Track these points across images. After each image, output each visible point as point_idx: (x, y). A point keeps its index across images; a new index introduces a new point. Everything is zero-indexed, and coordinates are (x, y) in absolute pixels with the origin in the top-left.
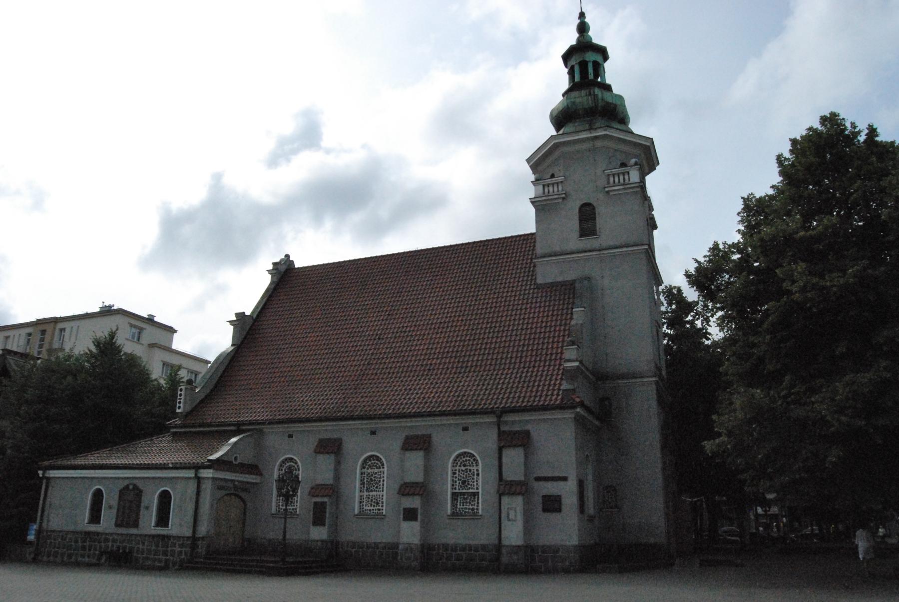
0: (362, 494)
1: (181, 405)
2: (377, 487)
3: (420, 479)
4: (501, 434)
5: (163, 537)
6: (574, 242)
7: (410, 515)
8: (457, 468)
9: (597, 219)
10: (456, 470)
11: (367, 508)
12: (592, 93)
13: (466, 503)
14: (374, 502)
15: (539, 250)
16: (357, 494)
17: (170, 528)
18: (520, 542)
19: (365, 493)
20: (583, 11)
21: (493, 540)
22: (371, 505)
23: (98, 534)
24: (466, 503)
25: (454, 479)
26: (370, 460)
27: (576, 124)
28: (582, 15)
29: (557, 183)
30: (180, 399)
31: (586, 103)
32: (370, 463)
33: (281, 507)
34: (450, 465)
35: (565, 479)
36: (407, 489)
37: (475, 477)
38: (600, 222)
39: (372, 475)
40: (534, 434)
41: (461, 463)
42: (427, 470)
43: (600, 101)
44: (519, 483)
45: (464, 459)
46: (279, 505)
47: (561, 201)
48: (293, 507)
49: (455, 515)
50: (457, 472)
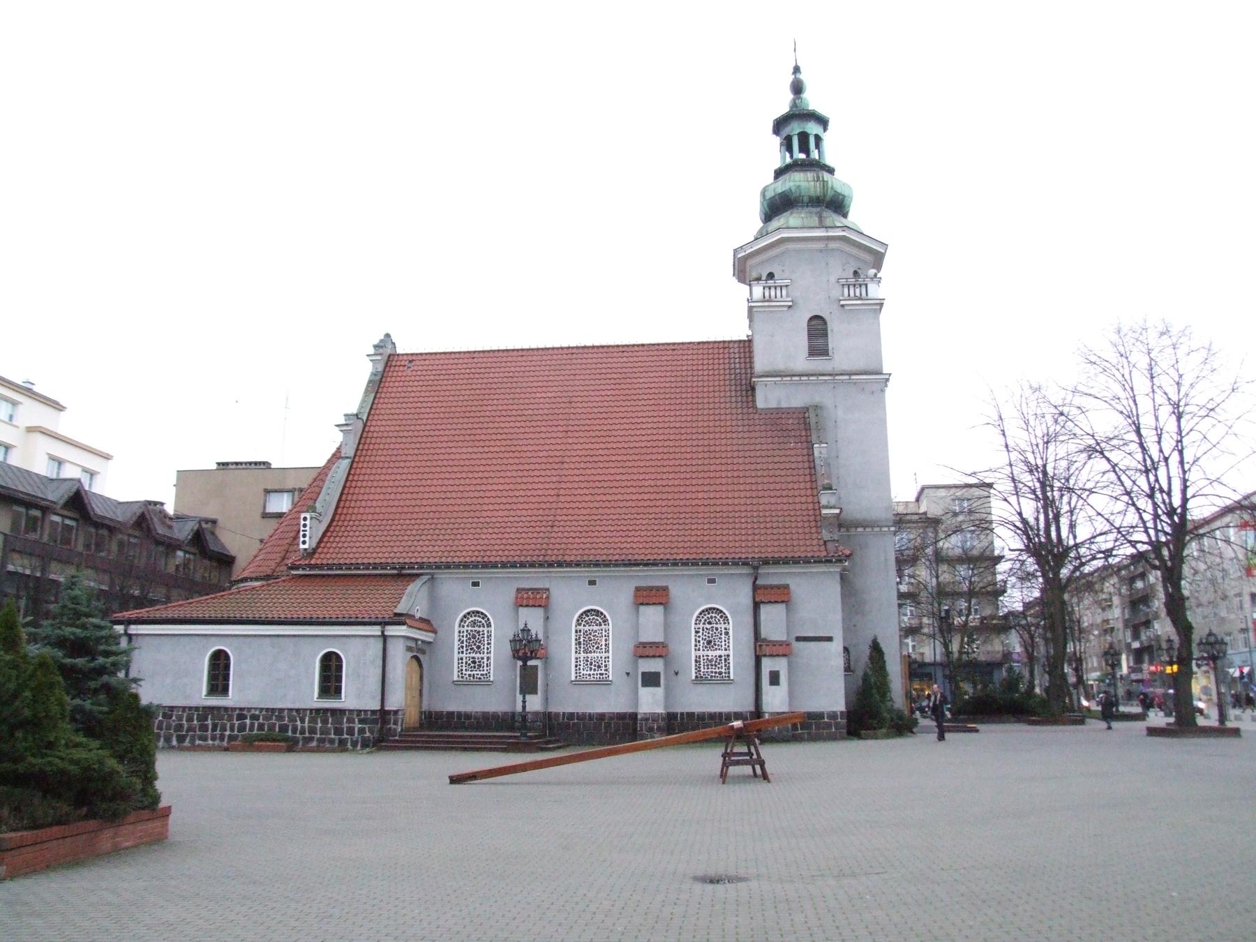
1: (307, 539)
2: (598, 648)
3: (659, 638)
4: (755, 588)
5: (334, 712)
6: (800, 360)
7: (651, 680)
8: (701, 626)
9: (829, 336)
10: (699, 628)
11: (585, 672)
12: (821, 179)
13: (712, 665)
14: (595, 666)
15: (760, 364)
16: (573, 656)
17: (343, 700)
19: (582, 654)
20: (798, 64)
21: (747, 706)
22: (591, 669)
23: (226, 709)
24: (712, 665)
25: (698, 639)
27: (803, 215)
28: (797, 70)
29: (781, 287)
30: (303, 531)
31: (812, 190)
32: (587, 619)
33: (464, 672)
34: (693, 622)
35: (830, 639)
36: (645, 650)
37: (723, 636)
38: (833, 342)
39: (590, 634)
40: (792, 587)
41: (705, 620)
42: (667, 626)
43: (829, 190)
44: (781, 643)
45: (709, 616)
46: (462, 670)
47: (786, 309)
48: (482, 672)
49: (699, 680)
50: (701, 630)
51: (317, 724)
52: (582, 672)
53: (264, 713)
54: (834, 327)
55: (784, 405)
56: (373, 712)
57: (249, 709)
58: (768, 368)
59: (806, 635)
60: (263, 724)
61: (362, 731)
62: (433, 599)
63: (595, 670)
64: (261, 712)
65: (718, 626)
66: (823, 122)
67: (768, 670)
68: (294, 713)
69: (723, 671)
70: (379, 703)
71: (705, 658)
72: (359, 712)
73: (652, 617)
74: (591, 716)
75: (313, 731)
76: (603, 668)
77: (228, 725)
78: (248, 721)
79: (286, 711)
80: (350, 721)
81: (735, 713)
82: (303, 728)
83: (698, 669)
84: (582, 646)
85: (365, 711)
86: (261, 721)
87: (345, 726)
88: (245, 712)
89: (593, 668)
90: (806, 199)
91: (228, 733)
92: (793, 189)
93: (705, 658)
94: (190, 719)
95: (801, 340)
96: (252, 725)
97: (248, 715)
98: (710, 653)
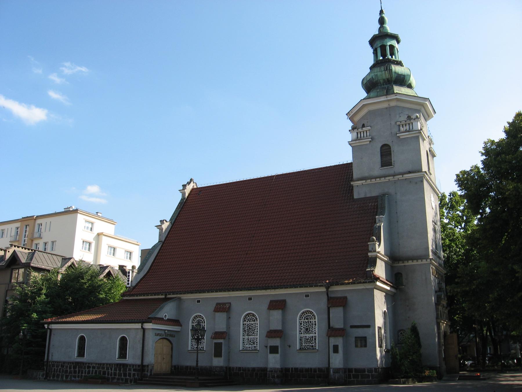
0: (244, 337)
3: (279, 328)
6: (377, 170)
7: (274, 350)
8: (303, 321)
10: (302, 322)
11: (247, 346)
13: (308, 342)
14: (252, 342)
17: (127, 360)
18: (341, 366)
24: (308, 342)
26: (249, 316)
28: (381, 12)
32: (248, 318)
36: (272, 334)
39: (250, 326)
41: (305, 317)
44: (339, 329)
46: (193, 345)
48: (202, 346)
50: (303, 323)
51: (117, 371)
52: (246, 346)
53: (97, 365)
54: (395, 149)
55: (368, 195)
56: (139, 366)
57: (92, 363)
58: (359, 176)
59: (356, 324)
60: (97, 371)
61: (134, 375)
62: (179, 308)
63: (252, 345)
64: (96, 365)
65: (312, 320)
66: (395, 37)
67: (333, 345)
68: (108, 366)
69: (314, 345)
70: (141, 361)
71: (305, 338)
72: (133, 365)
73: (277, 315)
74: (248, 369)
75: (115, 374)
76: (256, 344)
77: (84, 371)
78: (91, 369)
79: (105, 365)
80: (130, 370)
81: (319, 368)
82: (111, 373)
83: (301, 344)
84: (246, 332)
85: (136, 365)
86: (96, 369)
87: (128, 372)
88: (90, 365)
89: (251, 343)
90: (382, 81)
91: (83, 375)
92: (374, 77)
93: (305, 338)
94: (70, 368)
95: (377, 158)
96: (93, 371)
97: (91, 366)
98: (307, 335)
